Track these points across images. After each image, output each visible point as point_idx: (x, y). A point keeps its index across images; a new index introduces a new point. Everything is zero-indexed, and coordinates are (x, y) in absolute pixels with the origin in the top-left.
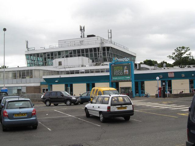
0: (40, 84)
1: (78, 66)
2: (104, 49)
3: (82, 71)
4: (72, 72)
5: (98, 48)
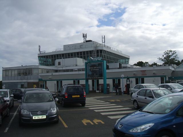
0: (38, 80)
1: (73, 66)
2: (98, 51)
3: (75, 70)
4: (67, 71)
5: (93, 51)
